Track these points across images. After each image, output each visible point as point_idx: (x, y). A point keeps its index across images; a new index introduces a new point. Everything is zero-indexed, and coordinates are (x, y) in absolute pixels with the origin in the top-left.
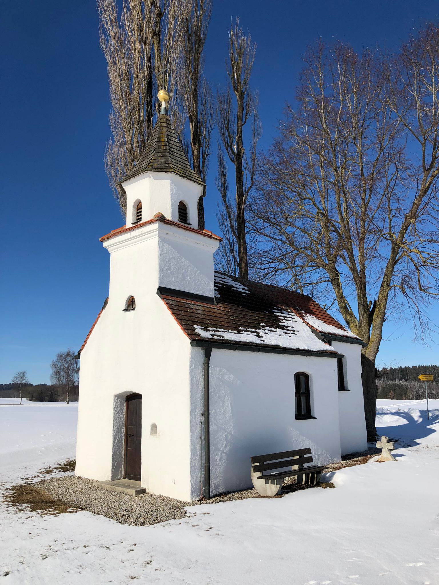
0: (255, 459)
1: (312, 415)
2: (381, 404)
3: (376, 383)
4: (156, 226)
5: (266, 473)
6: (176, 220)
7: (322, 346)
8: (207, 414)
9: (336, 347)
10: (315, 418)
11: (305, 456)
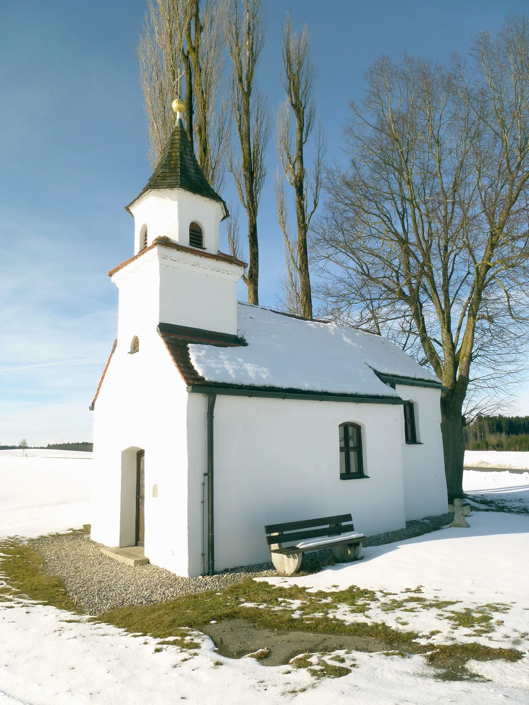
0: (270, 529)
1: (365, 474)
2: (471, 457)
3: (459, 434)
4: (156, 249)
5: (285, 545)
6: (186, 242)
7: (385, 390)
8: (210, 474)
9: (404, 392)
10: (368, 477)
11: (343, 524)
